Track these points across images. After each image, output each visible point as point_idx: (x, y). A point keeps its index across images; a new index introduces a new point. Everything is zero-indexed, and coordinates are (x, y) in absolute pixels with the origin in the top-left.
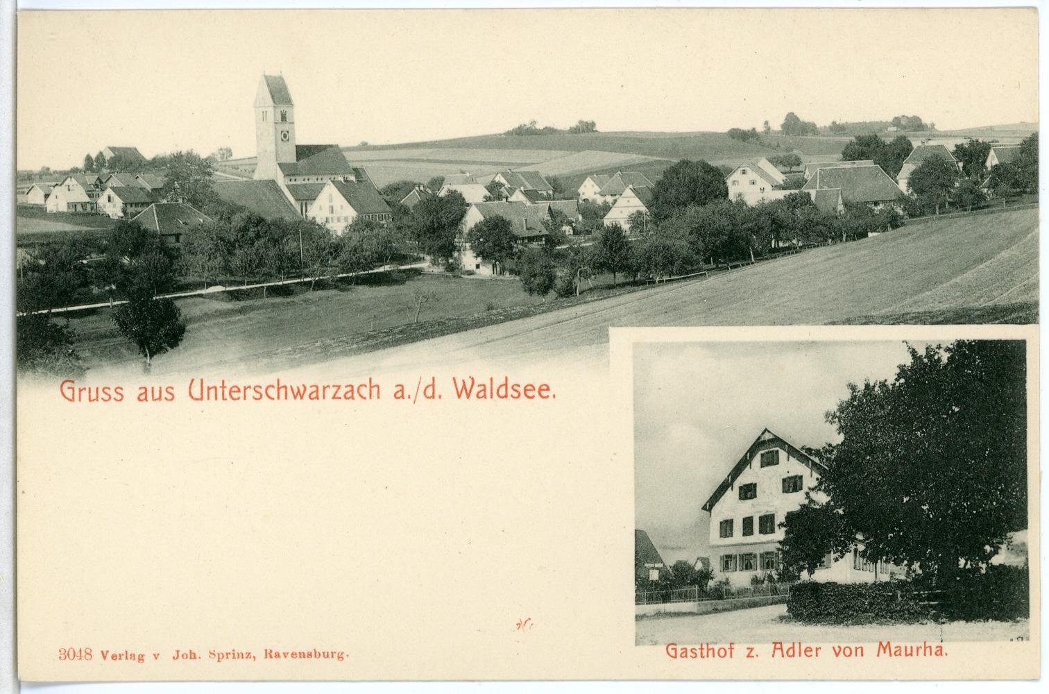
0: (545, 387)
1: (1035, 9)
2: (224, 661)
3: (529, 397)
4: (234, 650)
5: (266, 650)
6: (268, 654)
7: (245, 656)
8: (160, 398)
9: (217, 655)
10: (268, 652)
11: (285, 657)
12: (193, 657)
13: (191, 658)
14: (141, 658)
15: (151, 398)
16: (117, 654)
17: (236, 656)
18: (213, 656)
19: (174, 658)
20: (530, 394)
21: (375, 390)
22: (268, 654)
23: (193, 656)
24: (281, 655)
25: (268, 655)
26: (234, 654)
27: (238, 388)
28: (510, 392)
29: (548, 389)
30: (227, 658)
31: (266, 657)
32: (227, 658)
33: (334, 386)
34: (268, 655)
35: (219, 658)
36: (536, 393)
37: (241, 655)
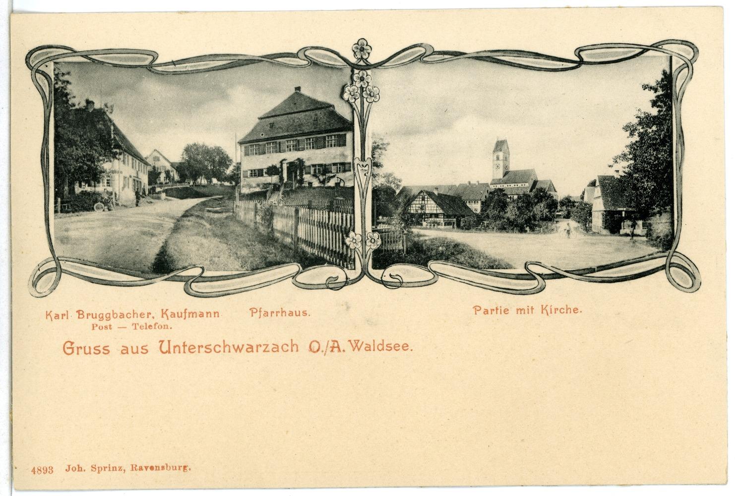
0: (406, 345)
1: (722, 7)
2: (102, 472)
3: (397, 350)
4: (109, 465)
5: (132, 465)
6: (134, 468)
7: (118, 469)
8: (137, 352)
9: (97, 468)
10: (134, 466)
11: (146, 470)
12: (80, 470)
13: (79, 471)
14: (93, 468)
15: (131, 351)
16: (154, 465)
17: (111, 469)
18: (94, 470)
19: (66, 470)
20: (397, 348)
21: (295, 348)
22: (134, 468)
23: (80, 469)
24: (144, 468)
25: (134, 469)
26: (110, 467)
27: (194, 346)
28: (385, 348)
29: (408, 346)
30: (105, 470)
31: (133, 470)
32: (105, 470)
33: (264, 345)
34: (134, 469)
35: (99, 471)
36: (401, 348)
37: (114, 469)
